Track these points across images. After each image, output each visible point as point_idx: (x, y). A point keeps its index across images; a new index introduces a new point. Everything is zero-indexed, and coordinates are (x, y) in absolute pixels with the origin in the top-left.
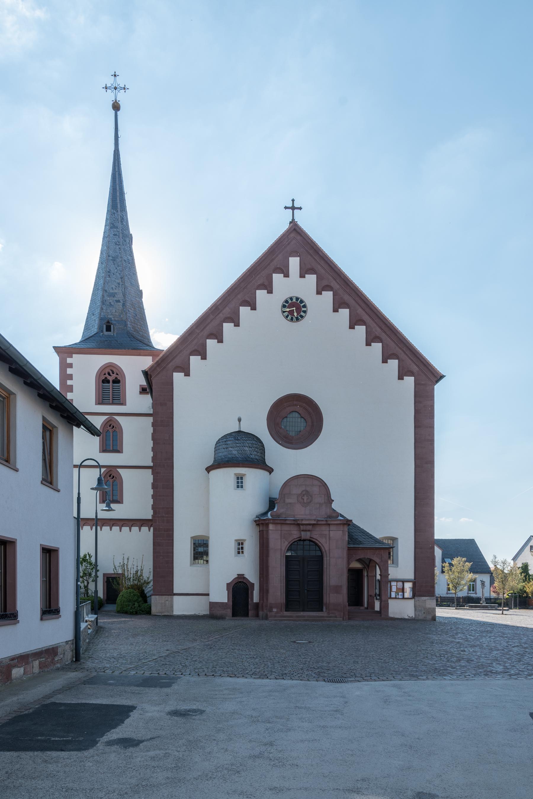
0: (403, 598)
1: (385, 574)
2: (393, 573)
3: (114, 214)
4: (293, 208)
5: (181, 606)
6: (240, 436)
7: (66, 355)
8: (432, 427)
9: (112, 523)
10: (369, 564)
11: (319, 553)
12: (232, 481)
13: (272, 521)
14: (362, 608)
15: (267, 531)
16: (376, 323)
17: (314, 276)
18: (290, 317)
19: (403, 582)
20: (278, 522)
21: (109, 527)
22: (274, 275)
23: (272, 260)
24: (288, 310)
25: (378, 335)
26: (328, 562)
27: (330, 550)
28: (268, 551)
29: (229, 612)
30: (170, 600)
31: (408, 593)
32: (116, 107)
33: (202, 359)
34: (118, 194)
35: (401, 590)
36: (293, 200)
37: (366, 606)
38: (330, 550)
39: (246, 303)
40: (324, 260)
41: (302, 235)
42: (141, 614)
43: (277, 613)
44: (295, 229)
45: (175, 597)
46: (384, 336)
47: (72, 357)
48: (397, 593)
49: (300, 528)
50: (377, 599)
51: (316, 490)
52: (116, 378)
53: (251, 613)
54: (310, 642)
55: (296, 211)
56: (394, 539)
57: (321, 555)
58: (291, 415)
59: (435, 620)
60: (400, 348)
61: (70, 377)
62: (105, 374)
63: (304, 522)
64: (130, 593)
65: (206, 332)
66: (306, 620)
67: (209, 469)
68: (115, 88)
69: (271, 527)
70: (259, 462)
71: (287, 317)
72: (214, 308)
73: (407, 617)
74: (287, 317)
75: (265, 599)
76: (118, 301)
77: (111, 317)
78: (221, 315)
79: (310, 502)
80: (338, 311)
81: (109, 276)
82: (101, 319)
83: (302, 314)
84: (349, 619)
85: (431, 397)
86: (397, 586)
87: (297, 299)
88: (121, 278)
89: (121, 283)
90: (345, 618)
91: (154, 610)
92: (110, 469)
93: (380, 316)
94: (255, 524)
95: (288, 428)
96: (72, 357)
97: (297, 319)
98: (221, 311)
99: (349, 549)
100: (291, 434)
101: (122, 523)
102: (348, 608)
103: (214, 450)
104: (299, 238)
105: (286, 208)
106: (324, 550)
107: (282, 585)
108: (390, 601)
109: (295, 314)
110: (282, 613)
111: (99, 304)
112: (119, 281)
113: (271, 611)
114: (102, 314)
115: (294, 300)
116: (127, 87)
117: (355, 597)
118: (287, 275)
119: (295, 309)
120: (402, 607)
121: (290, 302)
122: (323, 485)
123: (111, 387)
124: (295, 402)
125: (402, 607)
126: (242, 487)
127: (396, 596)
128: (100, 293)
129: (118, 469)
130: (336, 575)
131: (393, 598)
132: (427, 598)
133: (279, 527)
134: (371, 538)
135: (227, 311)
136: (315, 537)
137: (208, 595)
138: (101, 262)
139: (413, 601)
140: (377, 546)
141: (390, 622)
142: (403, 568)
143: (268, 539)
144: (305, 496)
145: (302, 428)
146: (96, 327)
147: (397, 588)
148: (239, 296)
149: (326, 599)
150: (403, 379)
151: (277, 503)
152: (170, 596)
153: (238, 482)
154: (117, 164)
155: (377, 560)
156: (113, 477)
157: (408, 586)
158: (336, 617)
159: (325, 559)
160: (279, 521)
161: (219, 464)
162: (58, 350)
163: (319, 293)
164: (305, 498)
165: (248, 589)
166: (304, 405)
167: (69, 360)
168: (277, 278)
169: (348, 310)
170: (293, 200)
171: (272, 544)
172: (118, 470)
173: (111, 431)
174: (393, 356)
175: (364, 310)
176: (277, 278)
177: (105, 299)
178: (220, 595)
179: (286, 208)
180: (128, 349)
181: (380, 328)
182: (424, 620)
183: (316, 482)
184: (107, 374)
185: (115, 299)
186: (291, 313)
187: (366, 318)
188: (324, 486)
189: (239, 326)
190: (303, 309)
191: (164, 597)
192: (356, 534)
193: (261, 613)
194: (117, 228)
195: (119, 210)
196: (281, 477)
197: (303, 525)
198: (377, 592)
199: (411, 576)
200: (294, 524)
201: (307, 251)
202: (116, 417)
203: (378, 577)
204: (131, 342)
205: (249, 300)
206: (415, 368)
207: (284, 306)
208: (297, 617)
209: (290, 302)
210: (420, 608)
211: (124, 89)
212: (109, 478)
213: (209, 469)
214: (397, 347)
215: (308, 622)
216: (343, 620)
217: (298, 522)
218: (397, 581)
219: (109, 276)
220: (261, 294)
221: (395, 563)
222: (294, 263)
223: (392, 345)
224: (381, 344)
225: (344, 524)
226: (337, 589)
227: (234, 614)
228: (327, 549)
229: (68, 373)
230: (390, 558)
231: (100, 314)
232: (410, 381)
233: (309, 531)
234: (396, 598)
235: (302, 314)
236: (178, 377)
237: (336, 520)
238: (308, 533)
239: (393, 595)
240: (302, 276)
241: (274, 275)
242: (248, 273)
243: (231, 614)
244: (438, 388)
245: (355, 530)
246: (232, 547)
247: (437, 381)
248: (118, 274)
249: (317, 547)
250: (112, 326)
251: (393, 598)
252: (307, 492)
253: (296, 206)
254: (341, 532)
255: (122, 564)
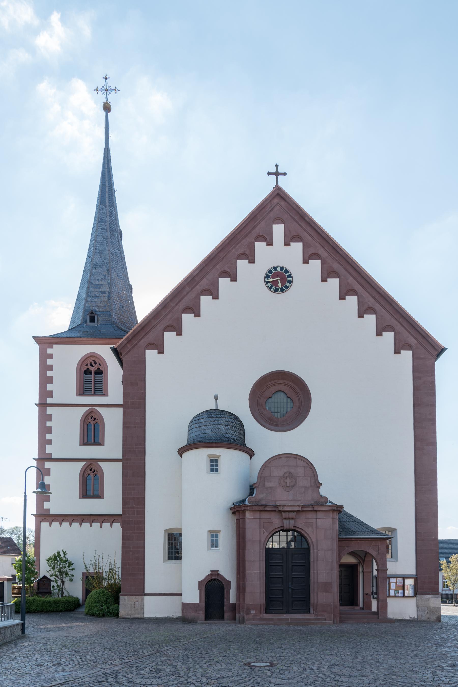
0: (404, 596)
1: (382, 569)
2: (392, 568)
3: (103, 209)
4: (277, 174)
5: (153, 608)
6: (214, 414)
7: (47, 345)
8: (434, 405)
9: (92, 519)
10: (364, 558)
11: (305, 546)
12: (205, 464)
13: (248, 508)
14: (357, 608)
15: (244, 519)
16: (369, 293)
17: (301, 244)
18: (273, 288)
19: (404, 578)
20: (257, 508)
21: (89, 523)
22: (256, 243)
23: (254, 228)
24: (271, 280)
25: (371, 305)
26: (315, 555)
27: (317, 540)
28: (244, 543)
29: (202, 614)
30: (140, 600)
31: (409, 591)
32: (107, 108)
33: (177, 335)
34: (107, 190)
35: (401, 588)
36: (277, 166)
37: (361, 605)
38: (317, 540)
39: (225, 274)
40: (311, 226)
41: (287, 200)
42: (108, 617)
43: (255, 615)
44: (278, 194)
45: (146, 597)
46: (377, 307)
47: (52, 348)
48: (396, 591)
49: (282, 515)
50: (373, 598)
51: (300, 471)
52: (99, 369)
53: (226, 615)
54: (272, 665)
55: (280, 177)
56: (393, 530)
57: (307, 547)
58: (276, 395)
59: (440, 621)
60: (396, 319)
61: (51, 368)
62: (87, 365)
63: (286, 508)
64: (100, 593)
65: (182, 305)
66: (289, 624)
67: (181, 451)
68: (106, 90)
69: (248, 515)
70: (238, 442)
71: (270, 288)
72: (190, 279)
73: (408, 618)
74: (270, 288)
75: (241, 600)
76: (104, 293)
77: (96, 308)
78: (198, 287)
79: (294, 486)
80: (326, 281)
81: (95, 268)
82: (85, 311)
83: (287, 284)
84: (341, 622)
85: (432, 372)
86: (396, 583)
87: (282, 268)
88: (108, 270)
89: (107, 275)
90: (335, 620)
91: (122, 612)
92: (90, 463)
93: (373, 284)
94: (231, 512)
95: (273, 410)
96: (52, 348)
97: (282, 290)
98: (199, 282)
99: (340, 540)
100: (276, 415)
101: (103, 518)
102: (340, 608)
103: (187, 430)
104: (283, 203)
105: (269, 174)
106: (310, 542)
107: (262, 582)
108: (389, 600)
109: (280, 285)
110: (261, 616)
111: (84, 296)
112: (106, 273)
113: (248, 613)
114: (87, 305)
115: (279, 270)
116: (118, 88)
117: (349, 594)
118: (270, 244)
119: (279, 279)
120: (402, 607)
121: (274, 271)
122: (309, 466)
123: (93, 378)
124: (280, 381)
125: (402, 607)
126: (216, 470)
127: (395, 594)
128: (86, 285)
129: (99, 463)
130: (325, 570)
131: (392, 597)
132: (430, 596)
133: (257, 515)
134: (366, 528)
135: (204, 283)
136: (300, 526)
137: (180, 594)
138: (89, 257)
139: (415, 599)
140: (373, 536)
141: (389, 625)
142: (403, 561)
143: (244, 529)
144: (288, 479)
145: (289, 409)
146: (80, 319)
147: (396, 585)
148: (218, 267)
149: (313, 599)
150: (399, 353)
151: (255, 487)
152: (140, 597)
153: (212, 465)
154: (106, 162)
155: (374, 553)
156: (94, 471)
157: (409, 582)
158: (325, 620)
159: (312, 551)
160: (259, 508)
161: (193, 444)
162: (38, 340)
163: (305, 261)
164: (288, 481)
165: (223, 588)
166: (291, 383)
167: (49, 351)
168: (259, 246)
169: (337, 280)
170: (277, 166)
171: (249, 535)
172: (99, 463)
173: (92, 423)
174: (388, 328)
175: (355, 279)
176: (259, 246)
177: (90, 290)
178: (193, 596)
179: (269, 174)
180: (111, 338)
181: (374, 298)
182: (427, 622)
183: (300, 463)
184: (89, 365)
185: (101, 290)
186: (275, 283)
187: (357, 287)
188: (310, 467)
189: (217, 298)
190: (288, 279)
191: (133, 597)
192: (348, 523)
193: (237, 616)
194: (105, 222)
195: (107, 205)
196: (260, 459)
197: (285, 511)
198: (374, 589)
199: (412, 571)
200: (275, 511)
201: (291, 217)
202: (98, 409)
203: (375, 573)
204: (115, 332)
205: (228, 270)
206: (413, 341)
207: (267, 276)
208: (279, 620)
209: (274, 271)
210: (423, 608)
211: (115, 91)
212: (90, 472)
213: (181, 451)
214: (392, 319)
215: (291, 627)
216: (334, 623)
217: (280, 509)
218: (396, 577)
219: (95, 268)
220: (242, 264)
221: (394, 557)
222: (278, 231)
223: (387, 316)
224: (375, 315)
225: (334, 510)
226: (326, 587)
227: (207, 617)
228: (314, 540)
229: (48, 363)
230: (388, 552)
231: (85, 305)
232: (407, 355)
233: (293, 519)
234: (395, 597)
235: (287, 284)
236: (151, 355)
237: (323, 506)
238: (292, 522)
239: (392, 593)
240: (287, 244)
241: (257, 244)
242: (228, 241)
243: (203, 618)
244: (439, 364)
245: (347, 519)
246: (205, 539)
247: (438, 355)
248: (104, 266)
249: (302, 538)
250: (96, 317)
251: (392, 597)
252: (290, 473)
253: (280, 171)
254: (331, 520)
255: (93, 561)
